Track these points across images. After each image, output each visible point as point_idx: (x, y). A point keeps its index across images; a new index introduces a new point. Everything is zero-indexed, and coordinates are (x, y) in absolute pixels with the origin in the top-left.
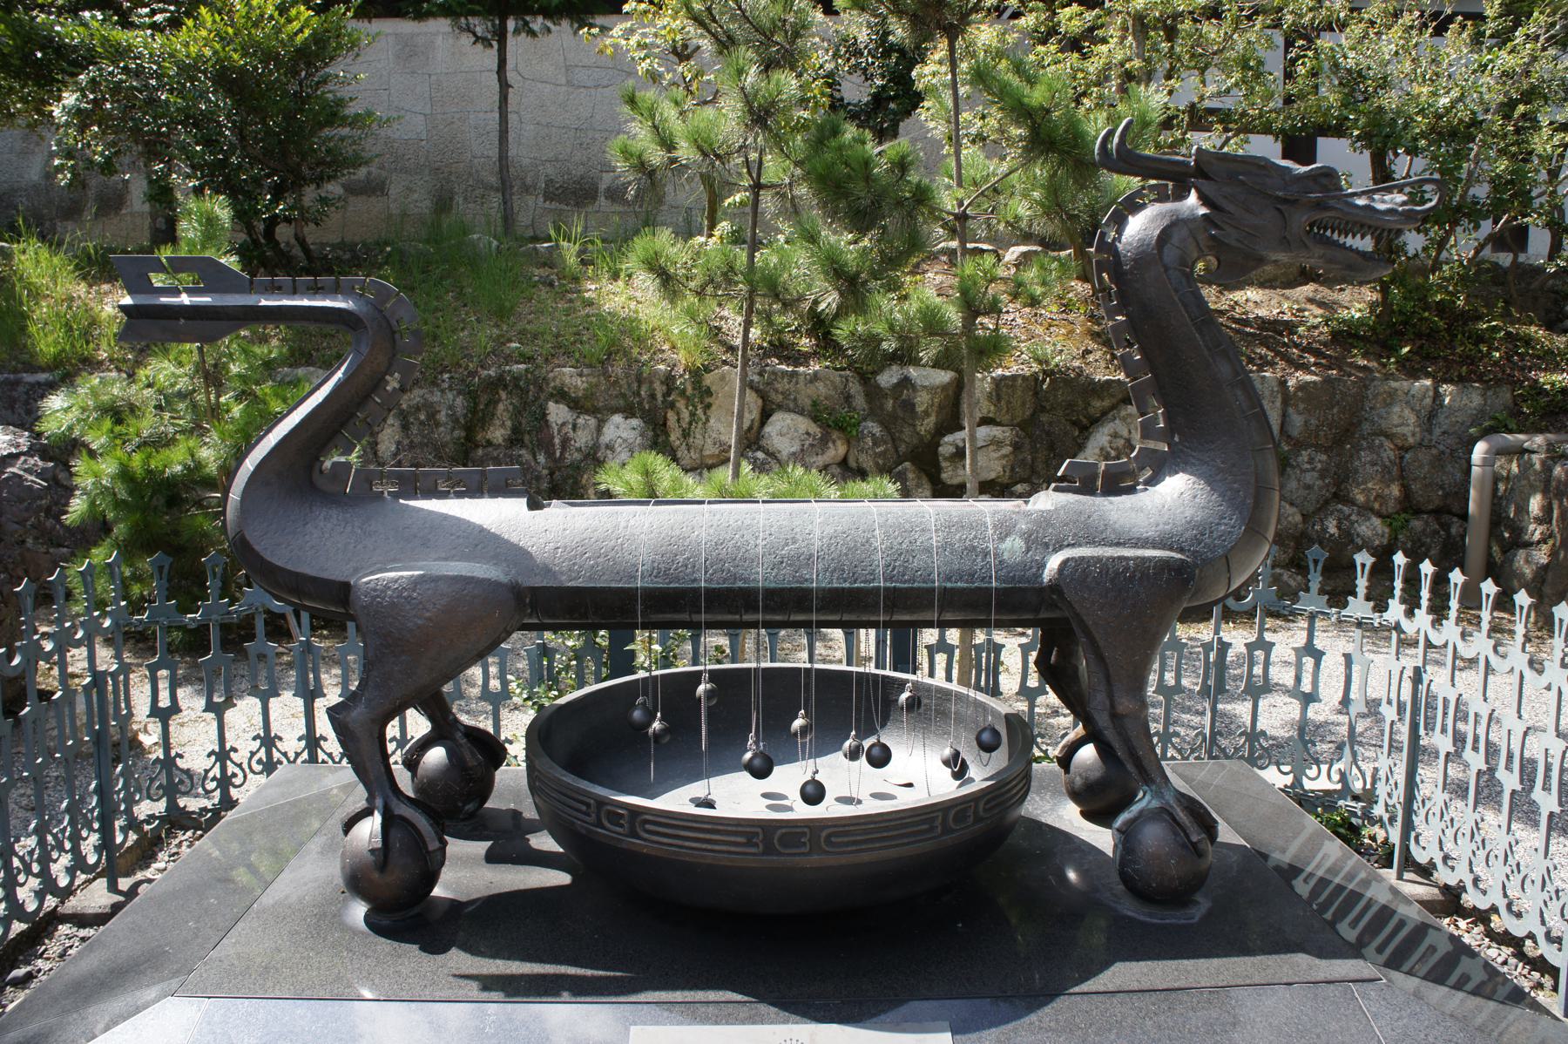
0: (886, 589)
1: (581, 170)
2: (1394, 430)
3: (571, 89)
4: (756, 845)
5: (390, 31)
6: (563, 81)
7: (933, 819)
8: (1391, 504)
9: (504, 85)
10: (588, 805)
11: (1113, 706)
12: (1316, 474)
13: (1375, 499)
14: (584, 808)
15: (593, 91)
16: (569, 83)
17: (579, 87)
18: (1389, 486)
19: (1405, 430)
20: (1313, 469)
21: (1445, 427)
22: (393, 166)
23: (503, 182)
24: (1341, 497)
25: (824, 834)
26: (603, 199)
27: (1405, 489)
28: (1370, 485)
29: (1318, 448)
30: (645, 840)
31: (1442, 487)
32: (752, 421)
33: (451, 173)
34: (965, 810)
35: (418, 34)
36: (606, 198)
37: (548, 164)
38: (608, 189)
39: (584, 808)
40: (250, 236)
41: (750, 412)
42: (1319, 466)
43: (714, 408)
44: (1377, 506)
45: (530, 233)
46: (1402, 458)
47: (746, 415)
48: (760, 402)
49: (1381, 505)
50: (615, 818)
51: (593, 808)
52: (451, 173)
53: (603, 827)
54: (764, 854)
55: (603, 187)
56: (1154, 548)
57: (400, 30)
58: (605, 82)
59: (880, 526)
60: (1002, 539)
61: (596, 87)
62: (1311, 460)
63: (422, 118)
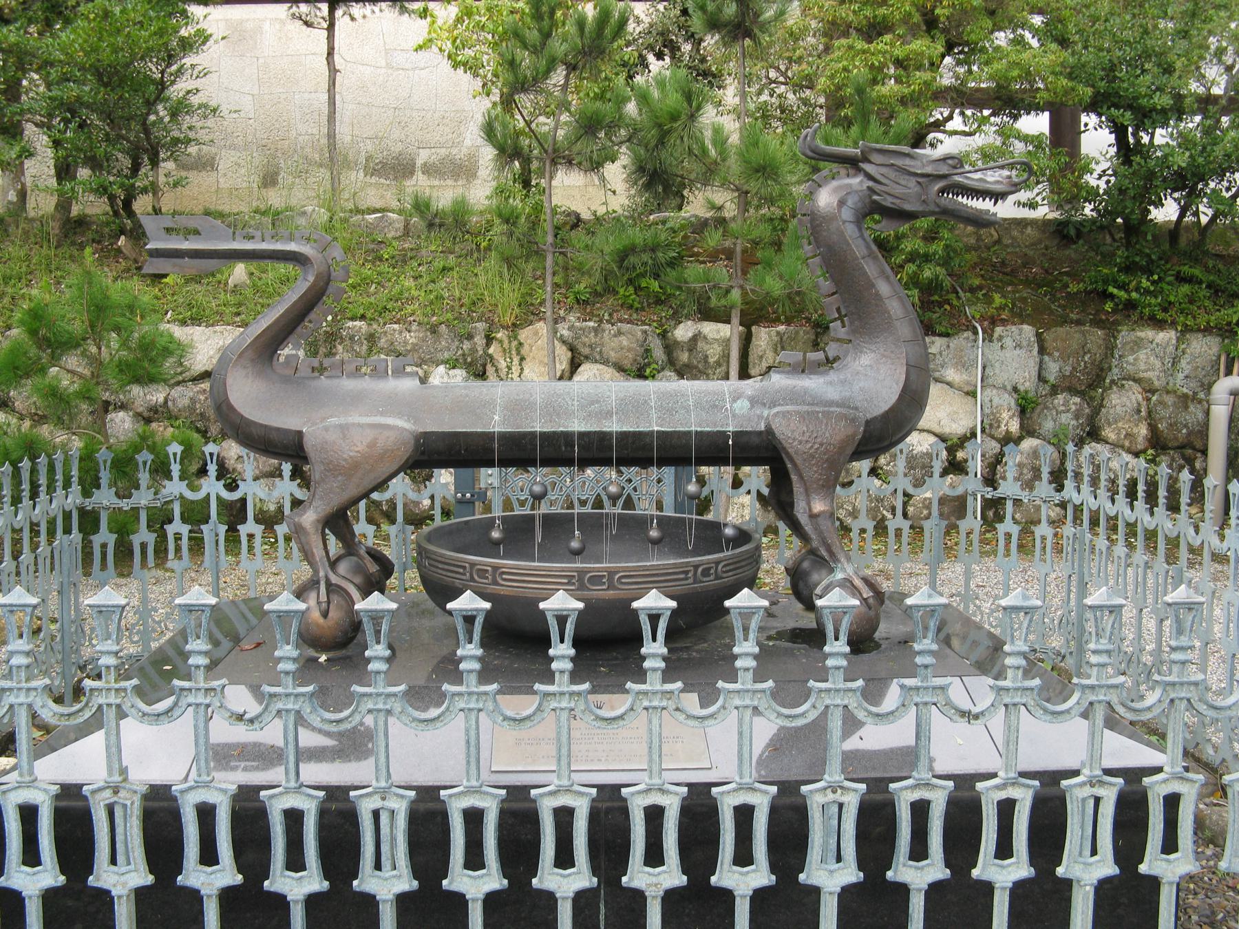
0: (658, 432)
1: (399, 147)
2: (1142, 375)
3: (390, 71)
4: (574, 584)
5: (221, 17)
6: (383, 63)
7: (686, 572)
8: (1140, 439)
9: (333, 71)
10: (464, 568)
11: (810, 510)
12: (1069, 415)
13: (1125, 436)
14: (461, 570)
15: (411, 73)
16: (389, 66)
17: (398, 69)
18: (1137, 425)
19: (1150, 374)
20: (1068, 411)
21: (1186, 372)
22: (222, 143)
23: (331, 159)
24: (1094, 434)
25: (617, 577)
26: (420, 173)
27: (1153, 428)
28: (1120, 425)
29: (1072, 391)
30: (503, 585)
31: (1186, 426)
32: (563, 371)
33: (277, 150)
34: (709, 569)
35: (248, 20)
36: (423, 173)
37: (368, 141)
38: (425, 164)
39: (461, 570)
40: (112, 207)
41: (561, 363)
42: (1073, 408)
43: (528, 360)
44: (1127, 444)
45: (351, 206)
46: (1148, 400)
47: (558, 366)
48: (569, 354)
49: (1131, 442)
50: (482, 573)
51: (468, 569)
52: (277, 150)
53: (475, 581)
54: (578, 589)
55: (419, 162)
56: (837, 407)
57: (229, 17)
58: (422, 65)
59: (654, 393)
60: (735, 400)
61: (414, 69)
62: (1066, 403)
63: (250, 98)
